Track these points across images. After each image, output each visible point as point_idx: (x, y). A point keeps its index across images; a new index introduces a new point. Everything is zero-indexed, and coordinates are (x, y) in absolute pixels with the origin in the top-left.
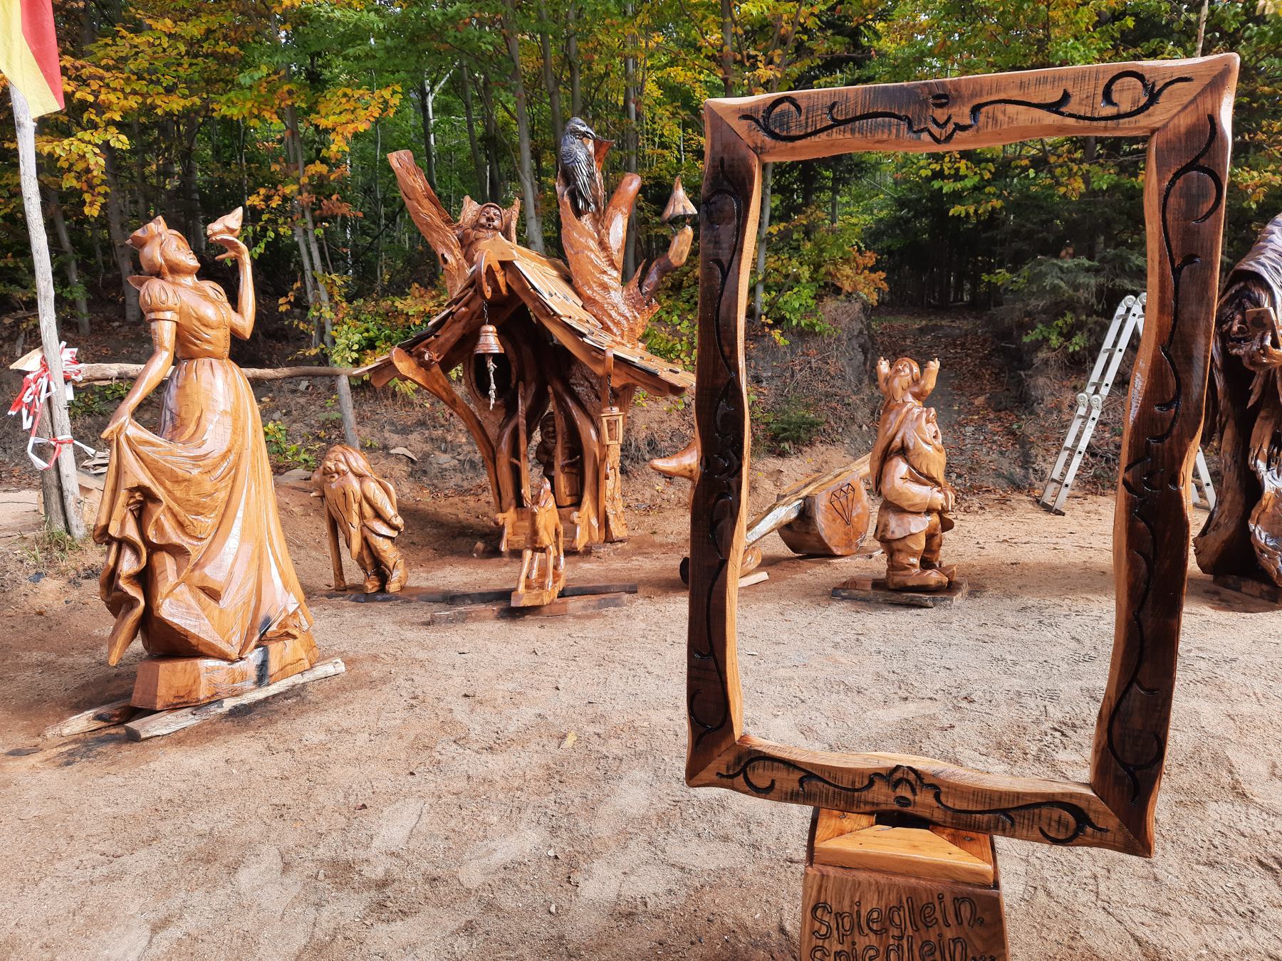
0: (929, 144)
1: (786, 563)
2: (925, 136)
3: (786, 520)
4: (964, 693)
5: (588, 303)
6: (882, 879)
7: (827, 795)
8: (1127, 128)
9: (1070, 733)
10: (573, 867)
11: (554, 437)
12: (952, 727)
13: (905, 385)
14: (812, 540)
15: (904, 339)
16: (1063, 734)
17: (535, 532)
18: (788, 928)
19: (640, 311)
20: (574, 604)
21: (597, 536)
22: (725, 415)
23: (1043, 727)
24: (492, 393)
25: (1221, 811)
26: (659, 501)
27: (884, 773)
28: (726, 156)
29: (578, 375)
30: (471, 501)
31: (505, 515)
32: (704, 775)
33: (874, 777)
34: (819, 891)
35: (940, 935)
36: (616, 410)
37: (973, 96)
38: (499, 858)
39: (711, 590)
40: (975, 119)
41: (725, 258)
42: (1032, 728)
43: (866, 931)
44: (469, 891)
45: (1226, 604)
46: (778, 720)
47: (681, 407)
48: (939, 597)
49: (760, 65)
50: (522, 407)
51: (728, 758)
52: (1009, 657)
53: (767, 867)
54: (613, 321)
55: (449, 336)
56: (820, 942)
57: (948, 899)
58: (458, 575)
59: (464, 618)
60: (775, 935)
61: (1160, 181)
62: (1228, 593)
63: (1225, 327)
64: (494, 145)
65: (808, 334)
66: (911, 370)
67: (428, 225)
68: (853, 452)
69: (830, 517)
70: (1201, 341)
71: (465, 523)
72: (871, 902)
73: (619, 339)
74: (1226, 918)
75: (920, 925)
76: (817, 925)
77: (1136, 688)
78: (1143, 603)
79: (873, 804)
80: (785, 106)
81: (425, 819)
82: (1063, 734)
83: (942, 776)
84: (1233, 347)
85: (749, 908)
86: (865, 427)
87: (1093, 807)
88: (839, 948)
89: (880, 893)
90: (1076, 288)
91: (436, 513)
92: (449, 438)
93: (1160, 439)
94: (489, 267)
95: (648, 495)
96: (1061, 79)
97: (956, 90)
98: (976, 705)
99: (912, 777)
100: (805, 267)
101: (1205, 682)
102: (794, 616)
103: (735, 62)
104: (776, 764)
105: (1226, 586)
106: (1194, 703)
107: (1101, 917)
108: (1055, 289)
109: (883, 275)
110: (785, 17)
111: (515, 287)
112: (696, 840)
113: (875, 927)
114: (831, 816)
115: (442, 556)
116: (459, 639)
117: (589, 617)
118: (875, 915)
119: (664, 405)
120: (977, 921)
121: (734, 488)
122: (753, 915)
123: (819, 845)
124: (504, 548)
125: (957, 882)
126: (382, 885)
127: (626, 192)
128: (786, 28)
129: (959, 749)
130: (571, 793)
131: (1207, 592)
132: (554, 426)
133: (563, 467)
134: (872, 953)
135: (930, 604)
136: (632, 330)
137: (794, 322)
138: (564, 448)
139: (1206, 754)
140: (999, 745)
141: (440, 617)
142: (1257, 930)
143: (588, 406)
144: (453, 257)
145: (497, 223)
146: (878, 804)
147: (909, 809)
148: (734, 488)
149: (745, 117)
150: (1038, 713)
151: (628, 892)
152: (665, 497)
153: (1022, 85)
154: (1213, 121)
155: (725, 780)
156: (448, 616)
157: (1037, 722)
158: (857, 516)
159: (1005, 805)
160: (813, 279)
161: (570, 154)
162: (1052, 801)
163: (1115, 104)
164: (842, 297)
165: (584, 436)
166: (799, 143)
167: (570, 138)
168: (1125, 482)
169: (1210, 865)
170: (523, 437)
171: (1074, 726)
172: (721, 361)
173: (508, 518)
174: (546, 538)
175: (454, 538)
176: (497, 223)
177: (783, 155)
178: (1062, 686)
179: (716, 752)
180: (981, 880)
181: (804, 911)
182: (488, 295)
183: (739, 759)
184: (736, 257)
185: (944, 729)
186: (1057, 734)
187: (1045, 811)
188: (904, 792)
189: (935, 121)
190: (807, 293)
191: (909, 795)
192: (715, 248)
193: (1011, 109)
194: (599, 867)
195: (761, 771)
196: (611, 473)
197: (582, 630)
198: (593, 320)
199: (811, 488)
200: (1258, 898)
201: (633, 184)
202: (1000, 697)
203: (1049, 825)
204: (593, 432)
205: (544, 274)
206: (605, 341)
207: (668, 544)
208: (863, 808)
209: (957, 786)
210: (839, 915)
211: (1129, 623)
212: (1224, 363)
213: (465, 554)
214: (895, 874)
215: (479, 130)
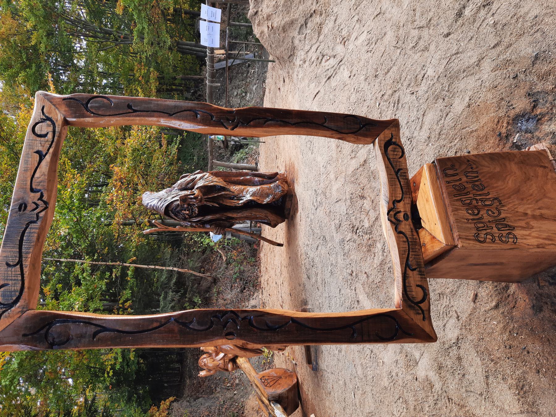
0: (46, 213)
1: (305, 408)
3: (281, 410)
4: (350, 277)
7: (415, 255)
9: (356, 228)
12: (366, 273)
13: (212, 360)
14: (291, 395)
15: (194, 384)
16: (357, 229)
18: (494, 304)
22: (199, 323)
27: (394, 227)
28: (23, 333)
33: (398, 232)
34: (470, 240)
39: (312, 329)
40: (37, 191)
41: (92, 329)
42: (358, 242)
43: (480, 216)
45: (296, 210)
46: (385, 360)
51: (412, 314)
52: (330, 268)
53: (466, 329)
60: (501, 310)
63: (187, 216)
66: (205, 358)
69: (278, 386)
72: (463, 213)
74: (414, 145)
75: (465, 191)
77: (326, 124)
78: (286, 122)
79: (412, 231)
82: (357, 229)
84: (195, 213)
85: (493, 329)
86: (235, 392)
87: (383, 139)
89: (457, 210)
97: (19, 200)
98: (353, 269)
99: (392, 213)
104: (407, 284)
105: (289, 214)
112: (466, 376)
118: (470, 212)
120: (453, 167)
121: (245, 314)
129: (375, 266)
131: (292, 220)
134: (490, 213)
139: (353, 179)
140: (369, 251)
142: (414, 135)
146: (412, 229)
147: (409, 214)
148: (245, 314)
150: (351, 243)
155: (426, 315)
157: (354, 241)
158: (276, 373)
159: (393, 172)
162: (385, 153)
163: (48, 133)
168: (233, 129)
171: (353, 227)
172: (162, 328)
178: (337, 240)
180: (432, 168)
183: (410, 307)
184: (94, 322)
185: (368, 277)
186: (358, 231)
192: (84, 337)
193: (37, 175)
195: (414, 293)
202: (348, 261)
203: (396, 155)
208: (416, 236)
209: (390, 192)
210: (478, 229)
212: (201, 216)
214: (445, 205)
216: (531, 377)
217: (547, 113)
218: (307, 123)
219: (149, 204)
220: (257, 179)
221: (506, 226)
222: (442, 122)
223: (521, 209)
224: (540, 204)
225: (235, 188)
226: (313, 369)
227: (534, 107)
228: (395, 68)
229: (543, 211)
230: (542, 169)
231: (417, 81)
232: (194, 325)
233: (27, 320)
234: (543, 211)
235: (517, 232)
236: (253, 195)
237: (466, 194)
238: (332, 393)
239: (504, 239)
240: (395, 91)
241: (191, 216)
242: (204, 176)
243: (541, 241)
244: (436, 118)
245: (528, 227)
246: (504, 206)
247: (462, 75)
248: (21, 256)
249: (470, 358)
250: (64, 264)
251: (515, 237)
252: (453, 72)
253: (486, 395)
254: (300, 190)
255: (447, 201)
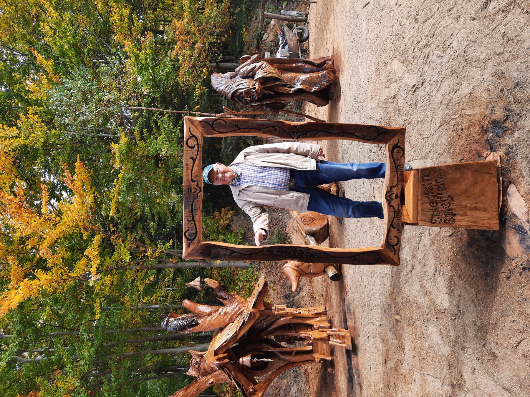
2: (199, 195)
3: (315, 241)
5: (231, 321)
6: (420, 203)
8: (201, 142)
10: (439, 312)
11: (284, 336)
14: (322, 232)
17: (322, 339)
18: (450, 234)
19: (235, 299)
20: (350, 323)
21: (324, 318)
23: (380, 154)
24: (266, 360)
25: (400, 102)
26: (309, 294)
29: (259, 325)
30: (312, 376)
31: (316, 358)
32: (395, 258)
34: (426, 221)
35: (435, 185)
36: (273, 308)
37: (189, 182)
38: (439, 341)
41: (230, 252)
43: (437, 207)
44: (452, 351)
45: (339, 97)
47: (272, 285)
48: (340, 186)
49: (146, 254)
50: (272, 350)
51: (388, 251)
54: (238, 310)
55: (243, 380)
56: (443, 221)
57: (423, 183)
58: (342, 380)
59: (357, 370)
60: (453, 238)
61: (215, 134)
62: (335, 96)
64: (161, 369)
65: (245, 236)
67: (197, 390)
68: (289, 218)
70: (258, 122)
71: (321, 379)
72: (427, 205)
73: (246, 308)
74: (431, 102)
76: (437, 222)
80: (187, 234)
81: (429, 372)
83: (387, 185)
88: (444, 215)
89: (424, 203)
90: (231, 143)
91: (316, 392)
92: (284, 387)
93: (285, 131)
94: (217, 360)
95: (307, 299)
96: (187, 159)
99: (388, 194)
100: (220, 237)
101: (362, 105)
102: (349, 237)
103: (143, 265)
105: (333, 97)
106: (369, 109)
107: (435, 137)
108: (231, 150)
109: (223, 209)
110: (130, 245)
111: (225, 350)
112: (426, 267)
113: (435, 204)
114: (404, 219)
115: (334, 388)
116: (366, 371)
117: (355, 317)
119: (271, 292)
120: (429, 175)
122: (448, 245)
123: (412, 222)
124: (330, 359)
125: (418, 181)
126: (453, 386)
127: (189, 305)
128: (134, 245)
130: (416, 314)
131: (335, 102)
132: (279, 336)
133: (296, 332)
134: (444, 205)
135: (343, 189)
136: (242, 303)
137: (240, 241)
138: (288, 332)
139: (384, 106)
141: (357, 381)
143: (271, 321)
144: (211, 379)
145: (198, 360)
147: (399, 195)
149: (189, 246)
151: (445, 290)
152: (308, 291)
153: (187, 169)
154: (201, 122)
156: (357, 377)
157: (378, 155)
159: (394, 168)
160: (224, 234)
161: (175, 328)
164: (231, 224)
165: (284, 323)
166: (198, 230)
167: (169, 328)
169: (416, 105)
170: (284, 349)
173: (317, 357)
174: (324, 335)
175: (326, 383)
176: (198, 360)
177: (200, 236)
179: (387, 255)
180: (416, 174)
181: (433, 226)
182: (228, 360)
183: (388, 248)
186: (381, 149)
187: (395, 156)
188: (394, 196)
189: (195, 192)
190: (229, 236)
191: (394, 195)
193: (193, 172)
194: (438, 301)
196: (298, 312)
197: (359, 319)
198: (238, 319)
199: (303, 232)
200: (424, 93)
201: (187, 303)
204: (282, 319)
205: (220, 338)
206: (246, 313)
207: (326, 289)
210: (433, 215)
211: (337, 136)
213: (333, 376)
215: (153, 375)
216: (456, 278)
217: (511, 129)
218: (343, 133)
219: (218, 88)
220: (307, 66)
221: (451, 213)
222: (452, 95)
223: (464, 204)
224: (478, 200)
225: (288, 75)
226: (339, 222)
227: (506, 120)
228: (431, 21)
229: (477, 205)
230: (488, 175)
231: (445, 46)
232: (275, 252)
233: (201, 246)
234: (477, 205)
235: (457, 218)
236: (304, 83)
237: (432, 193)
238: (350, 242)
239: (447, 221)
240: (427, 45)
241: (251, 101)
242: (262, 65)
243: (470, 223)
244: (449, 90)
245: (465, 215)
246: (453, 201)
247: (474, 64)
248: (193, 217)
249: (430, 258)
250: (145, 111)
251: (454, 221)
252: (469, 56)
253: (433, 279)
254: (344, 80)
255: (419, 197)
